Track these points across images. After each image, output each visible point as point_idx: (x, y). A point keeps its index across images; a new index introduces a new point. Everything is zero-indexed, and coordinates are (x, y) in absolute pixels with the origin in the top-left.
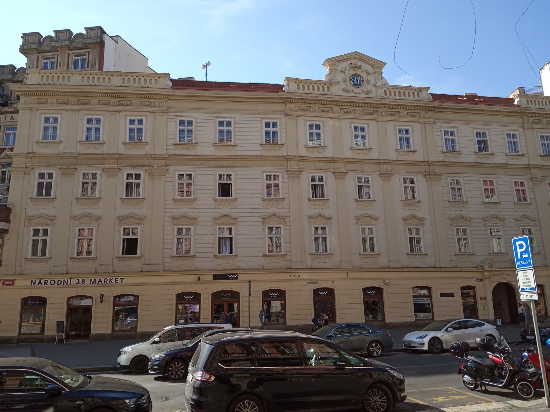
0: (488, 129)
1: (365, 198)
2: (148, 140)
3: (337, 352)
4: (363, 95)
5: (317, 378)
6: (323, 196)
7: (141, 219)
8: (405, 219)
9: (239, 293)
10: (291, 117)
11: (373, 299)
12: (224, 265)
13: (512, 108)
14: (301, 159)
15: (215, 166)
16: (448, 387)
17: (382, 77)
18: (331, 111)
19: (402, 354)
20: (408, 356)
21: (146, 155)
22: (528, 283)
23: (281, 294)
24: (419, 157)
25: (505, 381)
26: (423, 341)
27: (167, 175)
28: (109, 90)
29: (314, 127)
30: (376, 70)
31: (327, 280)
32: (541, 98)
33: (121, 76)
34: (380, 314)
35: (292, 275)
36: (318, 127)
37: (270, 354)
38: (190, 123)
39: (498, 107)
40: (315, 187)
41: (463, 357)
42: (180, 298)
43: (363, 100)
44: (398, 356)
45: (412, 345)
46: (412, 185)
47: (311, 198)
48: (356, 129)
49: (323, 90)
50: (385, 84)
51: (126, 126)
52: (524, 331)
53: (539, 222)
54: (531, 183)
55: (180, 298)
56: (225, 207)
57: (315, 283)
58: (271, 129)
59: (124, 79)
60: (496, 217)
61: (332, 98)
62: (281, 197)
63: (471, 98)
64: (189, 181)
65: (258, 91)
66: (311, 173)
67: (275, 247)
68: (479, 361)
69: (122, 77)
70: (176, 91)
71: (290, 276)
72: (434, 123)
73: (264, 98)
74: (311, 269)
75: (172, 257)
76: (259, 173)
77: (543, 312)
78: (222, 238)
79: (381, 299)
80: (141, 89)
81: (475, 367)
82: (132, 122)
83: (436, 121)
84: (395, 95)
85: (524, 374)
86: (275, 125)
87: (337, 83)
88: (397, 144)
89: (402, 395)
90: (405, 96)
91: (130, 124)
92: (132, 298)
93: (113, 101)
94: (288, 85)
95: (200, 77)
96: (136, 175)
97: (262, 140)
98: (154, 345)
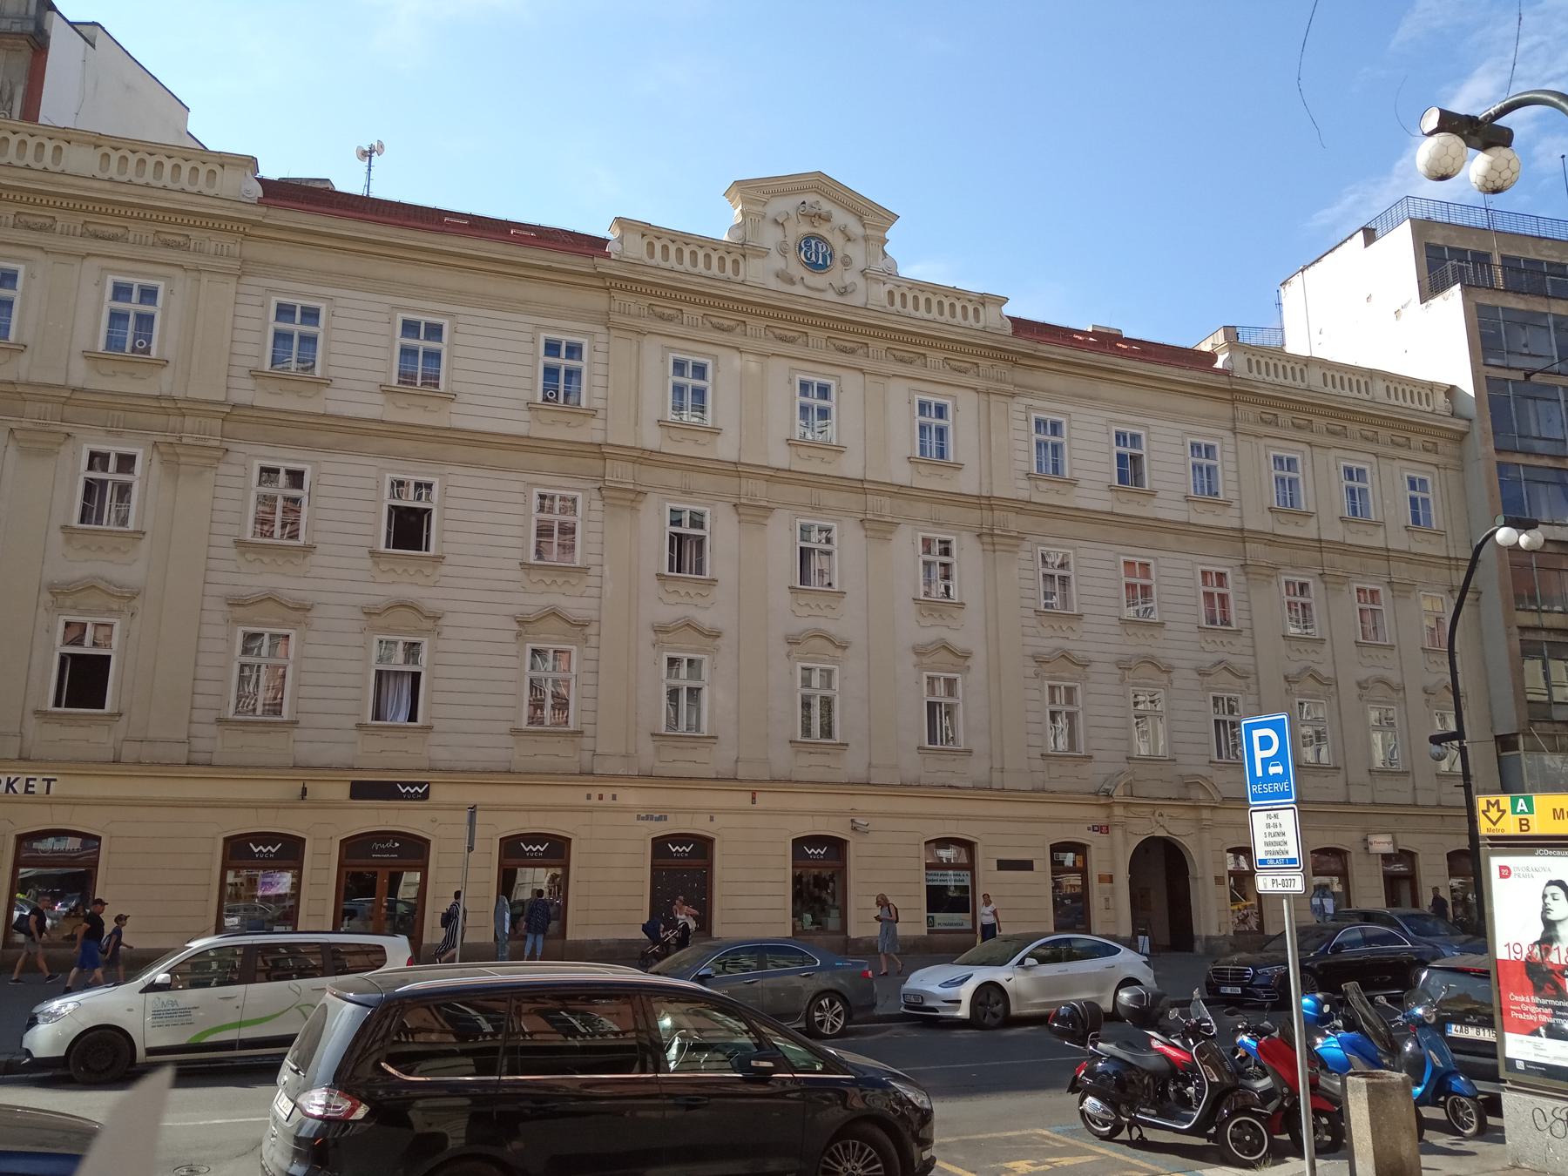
0: (1147, 426)
1: (815, 583)
2: (169, 354)
3: (751, 1029)
4: (831, 296)
5: (689, 1108)
6: (700, 569)
7: (128, 596)
8: (919, 651)
9: (427, 842)
10: (623, 334)
11: (816, 871)
12: (387, 754)
13: (1210, 376)
14: (644, 457)
15: (382, 454)
16: (1040, 1131)
17: (885, 254)
18: (738, 330)
19: (897, 1029)
20: (914, 1034)
21: (157, 398)
22: (1279, 844)
23: (557, 849)
24: (967, 483)
25: (1196, 1115)
26: (958, 993)
27: (223, 468)
28: (53, 184)
29: (689, 371)
30: (869, 232)
31: (695, 811)
32: (1276, 356)
33: (97, 146)
34: (834, 913)
35: (595, 793)
36: (700, 371)
37: (531, 1034)
38: (311, 315)
39: (1176, 371)
40: (678, 541)
41: (1084, 1045)
42: (238, 850)
43: (830, 310)
44: (887, 1034)
45: (928, 1004)
46: (945, 559)
47: (667, 572)
48: (805, 387)
49: (722, 268)
50: (890, 274)
51: (100, 303)
52: (1216, 971)
53: (1258, 683)
54: (1243, 579)
55: (238, 850)
56: (404, 580)
57: (659, 819)
58: (563, 362)
59: (106, 156)
60: (1150, 661)
61: (745, 293)
62: (578, 564)
63: (1107, 340)
64: (295, 493)
65: (531, 245)
66: (670, 500)
67: (548, 704)
68: (1129, 1059)
69: (100, 151)
70: (272, 212)
71: (589, 797)
72: (1013, 396)
73: (549, 269)
74: (648, 778)
75: (220, 721)
76: (518, 487)
77: (1253, 922)
78: (388, 672)
79: (842, 870)
80: (162, 193)
81: (1115, 1073)
82: (121, 292)
83: (1016, 390)
84: (916, 308)
85: (1244, 1096)
86: (574, 351)
87: (763, 253)
88: (913, 440)
89: (926, 1155)
90: (941, 313)
91: (115, 298)
92: (73, 844)
93: (62, 221)
94: (621, 240)
95: (348, 181)
96: (418, 485)
97: (532, 390)
98: (151, 996)
